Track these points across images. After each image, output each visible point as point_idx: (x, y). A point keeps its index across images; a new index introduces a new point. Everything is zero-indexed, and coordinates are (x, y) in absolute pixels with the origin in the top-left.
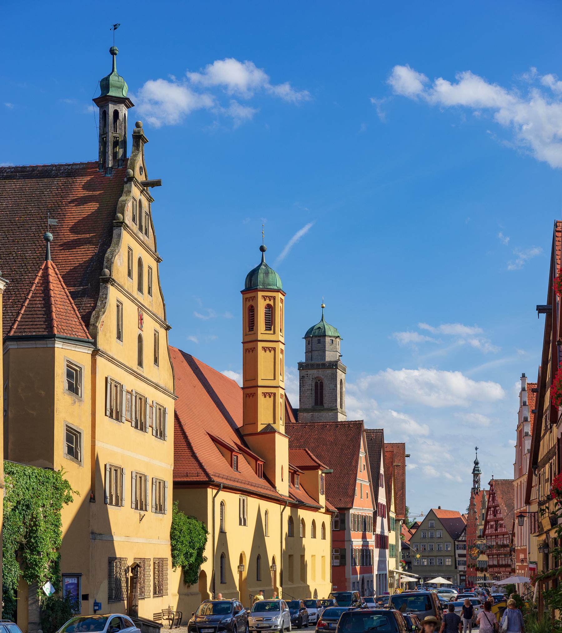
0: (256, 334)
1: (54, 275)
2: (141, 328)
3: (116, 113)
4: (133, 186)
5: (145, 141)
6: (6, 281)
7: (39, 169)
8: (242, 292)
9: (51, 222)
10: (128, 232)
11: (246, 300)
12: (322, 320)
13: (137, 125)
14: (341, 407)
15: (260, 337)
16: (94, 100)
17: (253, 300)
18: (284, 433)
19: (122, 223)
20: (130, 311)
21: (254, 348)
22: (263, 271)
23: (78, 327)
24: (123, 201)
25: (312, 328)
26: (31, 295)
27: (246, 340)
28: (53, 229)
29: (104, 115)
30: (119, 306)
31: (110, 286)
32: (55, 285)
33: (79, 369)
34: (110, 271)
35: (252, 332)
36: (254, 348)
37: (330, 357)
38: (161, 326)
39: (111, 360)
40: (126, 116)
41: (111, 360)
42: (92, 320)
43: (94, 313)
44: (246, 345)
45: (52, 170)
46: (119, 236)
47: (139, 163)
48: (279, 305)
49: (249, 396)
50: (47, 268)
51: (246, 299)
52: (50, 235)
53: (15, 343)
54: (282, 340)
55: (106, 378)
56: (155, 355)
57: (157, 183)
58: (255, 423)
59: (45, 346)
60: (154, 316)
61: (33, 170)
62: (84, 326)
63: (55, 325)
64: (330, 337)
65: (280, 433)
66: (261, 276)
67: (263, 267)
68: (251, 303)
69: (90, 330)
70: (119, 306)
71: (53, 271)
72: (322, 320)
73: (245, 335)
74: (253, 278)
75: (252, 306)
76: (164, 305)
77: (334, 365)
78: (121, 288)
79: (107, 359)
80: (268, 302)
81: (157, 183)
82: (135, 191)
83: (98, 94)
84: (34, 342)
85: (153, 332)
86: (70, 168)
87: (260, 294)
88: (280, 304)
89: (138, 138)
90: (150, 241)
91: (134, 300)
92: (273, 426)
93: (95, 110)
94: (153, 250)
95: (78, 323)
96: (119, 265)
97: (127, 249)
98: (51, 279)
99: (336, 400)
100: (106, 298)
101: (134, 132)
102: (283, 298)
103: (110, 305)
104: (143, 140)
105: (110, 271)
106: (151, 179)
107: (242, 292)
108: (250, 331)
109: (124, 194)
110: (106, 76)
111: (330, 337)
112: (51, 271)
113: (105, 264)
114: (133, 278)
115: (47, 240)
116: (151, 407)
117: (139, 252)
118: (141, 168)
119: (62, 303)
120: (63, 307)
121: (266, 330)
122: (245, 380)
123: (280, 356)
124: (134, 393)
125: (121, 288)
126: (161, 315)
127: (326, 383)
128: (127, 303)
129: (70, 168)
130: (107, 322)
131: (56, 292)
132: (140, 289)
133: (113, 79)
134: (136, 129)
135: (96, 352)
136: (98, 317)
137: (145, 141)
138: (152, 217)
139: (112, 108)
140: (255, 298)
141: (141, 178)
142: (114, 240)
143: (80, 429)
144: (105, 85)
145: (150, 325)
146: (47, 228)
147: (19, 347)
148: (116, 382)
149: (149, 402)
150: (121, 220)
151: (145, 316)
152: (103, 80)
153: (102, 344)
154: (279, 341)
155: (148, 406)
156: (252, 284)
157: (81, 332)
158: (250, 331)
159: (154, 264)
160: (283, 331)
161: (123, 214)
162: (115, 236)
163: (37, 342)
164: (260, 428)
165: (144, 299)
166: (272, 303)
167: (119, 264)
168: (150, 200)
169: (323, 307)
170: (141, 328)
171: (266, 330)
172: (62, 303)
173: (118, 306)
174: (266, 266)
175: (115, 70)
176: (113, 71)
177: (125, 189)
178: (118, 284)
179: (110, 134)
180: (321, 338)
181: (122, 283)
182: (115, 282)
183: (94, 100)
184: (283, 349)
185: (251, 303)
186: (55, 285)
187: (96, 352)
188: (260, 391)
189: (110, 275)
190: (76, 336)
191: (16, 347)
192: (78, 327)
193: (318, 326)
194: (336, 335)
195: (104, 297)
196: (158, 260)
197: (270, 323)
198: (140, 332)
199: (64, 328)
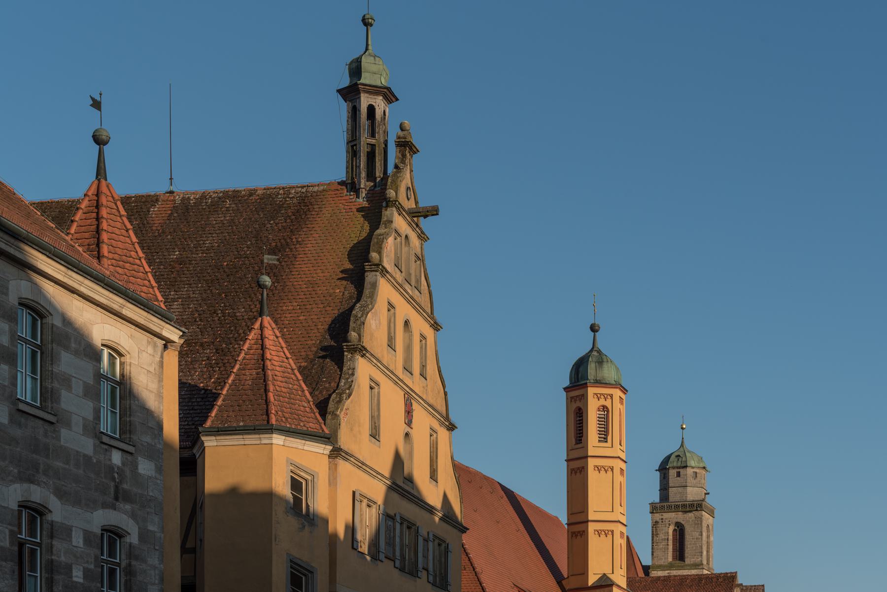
0: (585, 448)
1: (272, 337)
2: (409, 423)
3: (371, 109)
4: (396, 214)
5: (414, 150)
6: (183, 329)
7: (260, 192)
8: (565, 389)
9: (268, 259)
10: (389, 281)
11: (570, 400)
12: (682, 445)
13: (402, 128)
14: (708, 563)
15: (591, 452)
16: (339, 91)
17: (580, 400)
18: (625, 586)
19: (378, 265)
20: (392, 400)
21: (583, 468)
22: (594, 359)
23: (309, 415)
24: (380, 235)
25: (669, 457)
26: (237, 366)
27: (570, 457)
28: (271, 271)
29: (354, 111)
30: (374, 385)
31: (358, 357)
32: (273, 353)
33: (309, 478)
34: (359, 335)
35: (580, 446)
36: (583, 468)
37: (692, 494)
38: (442, 424)
39: (361, 465)
40: (387, 114)
41: (361, 465)
42: (331, 406)
43: (334, 396)
44: (571, 463)
45: (278, 194)
46: (374, 285)
47: (406, 180)
48: (617, 405)
49: (576, 536)
50: (262, 328)
51: (572, 398)
52: (267, 280)
53: (213, 438)
54: (623, 519)
55: (354, 493)
56: (431, 465)
57: (433, 211)
58: (584, 573)
59: (258, 442)
60: (431, 408)
61: (251, 195)
62: (317, 414)
63: (273, 412)
64: (693, 468)
65: (619, 587)
66: (592, 368)
67: (595, 353)
68: (578, 404)
69: (328, 421)
70: (374, 385)
71: (271, 333)
72: (682, 445)
73: (569, 450)
74: (581, 369)
75: (580, 409)
76: (446, 394)
77: (697, 506)
78: (376, 361)
79: (355, 465)
80: (602, 402)
81: (433, 211)
82: (400, 223)
83: (346, 82)
84: (241, 437)
85: (428, 431)
86: (304, 190)
87: (591, 391)
88: (619, 406)
89: (406, 146)
90: (424, 300)
91: (398, 382)
92: (611, 576)
93: (343, 107)
94: (429, 311)
95: (308, 409)
96: (374, 327)
97: (386, 305)
98: (268, 343)
99: (702, 553)
100: (353, 374)
101: (399, 138)
102: (623, 396)
103: (359, 386)
104: (411, 149)
105: (359, 335)
106: (424, 203)
107: (565, 389)
108: (577, 443)
109: (382, 226)
110: (357, 56)
111: (693, 468)
112: (268, 332)
113: (352, 324)
114: (397, 350)
115: (261, 286)
116: (426, 540)
117: (404, 310)
118: (408, 189)
119: (284, 380)
120: (286, 385)
121: (599, 441)
122: (570, 514)
123: (618, 478)
124: (398, 518)
125: (376, 361)
126: (441, 406)
127: (688, 530)
128: (387, 388)
129: (304, 190)
130: (354, 413)
131: (276, 363)
132: (408, 369)
133: (366, 62)
134: (401, 134)
135: (337, 453)
136: (340, 401)
137: (414, 150)
138: (426, 262)
139: (365, 101)
140: (584, 397)
141: (410, 205)
142: (367, 292)
143: (312, 567)
144: (356, 69)
145: (423, 420)
146: (261, 268)
147: (219, 444)
148: (369, 500)
149: (423, 532)
150: (377, 262)
151: (415, 406)
152: (352, 62)
153: (345, 440)
154: (619, 457)
155: (421, 540)
156: (579, 379)
157: (313, 423)
158: (577, 443)
159: (429, 332)
160: (624, 503)
161: (380, 253)
162: (367, 285)
163: (245, 436)
164: (592, 580)
165: (416, 383)
166: (608, 403)
167: (373, 326)
168: (423, 237)
169: (682, 428)
170: (409, 423)
171: (599, 441)
172: (284, 380)
173: (371, 388)
174: (599, 352)
175: (370, 47)
176: (367, 49)
177: (384, 219)
178: (372, 355)
179: (363, 139)
180: (681, 470)
181: (379, 356)
182: (365, 349)
183: (339, 91)
184: (624, 468)
185: (578, 404)
186: (273, 353)
187: (337, 453)
188: (592, 527)
189: (360, 340)
190: (305, 429)
191: (215, 444)
192: (309, 415)
193: (677, 454)
194: (701, 465)
195: (350, 372)
196: (436, 327)
197: (604, 435)
198: (408, 429)
199: (287, 415)
